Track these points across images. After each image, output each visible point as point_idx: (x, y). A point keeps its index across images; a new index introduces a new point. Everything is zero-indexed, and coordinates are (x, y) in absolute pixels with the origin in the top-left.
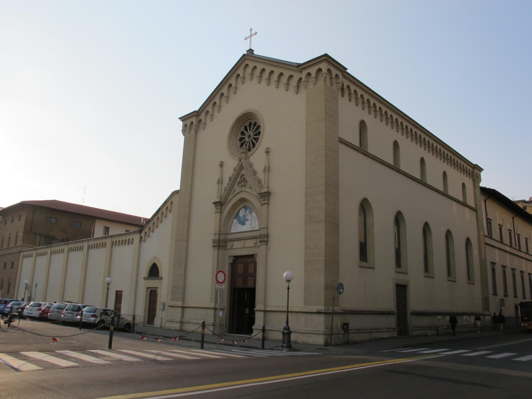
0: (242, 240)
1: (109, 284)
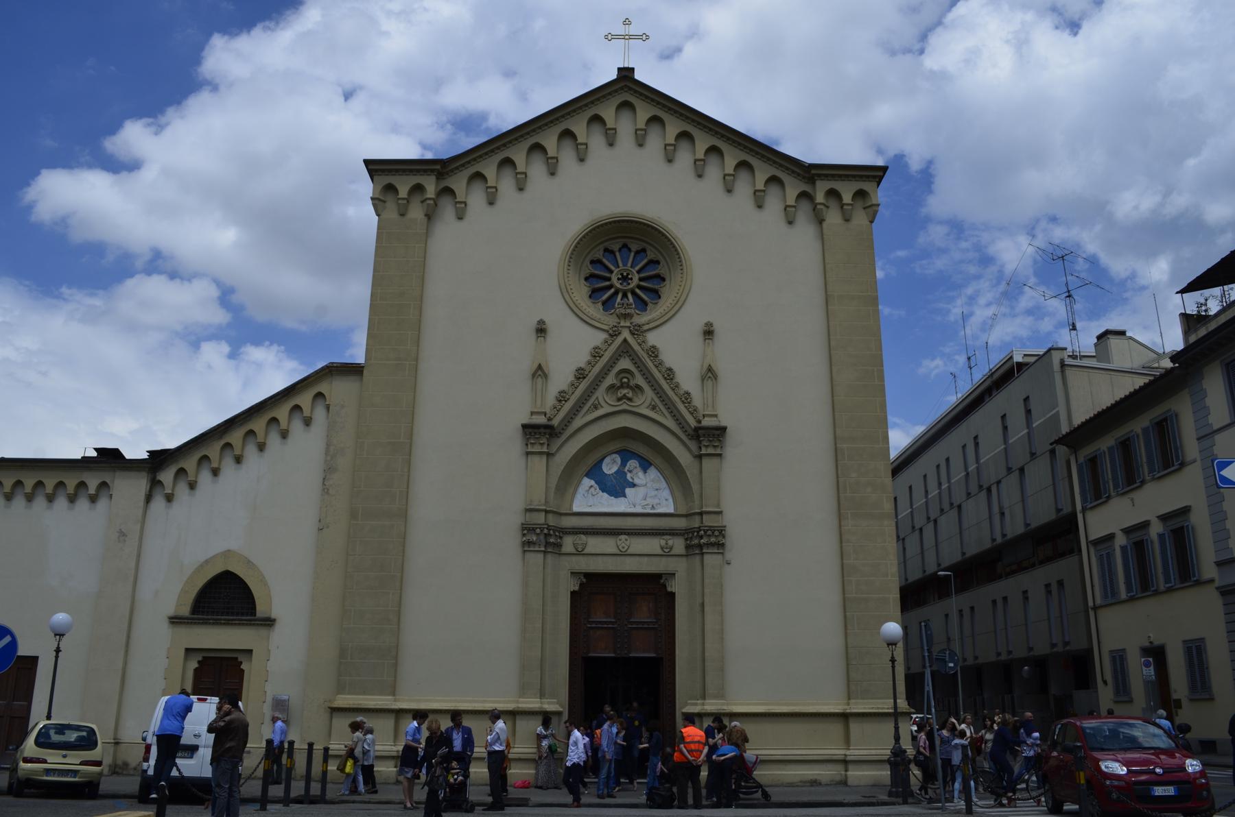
0: (664, 534)
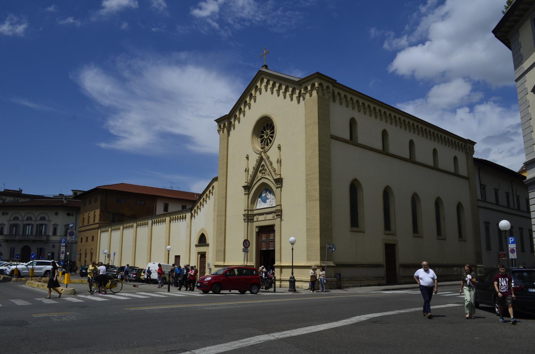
1: (169, 251)
